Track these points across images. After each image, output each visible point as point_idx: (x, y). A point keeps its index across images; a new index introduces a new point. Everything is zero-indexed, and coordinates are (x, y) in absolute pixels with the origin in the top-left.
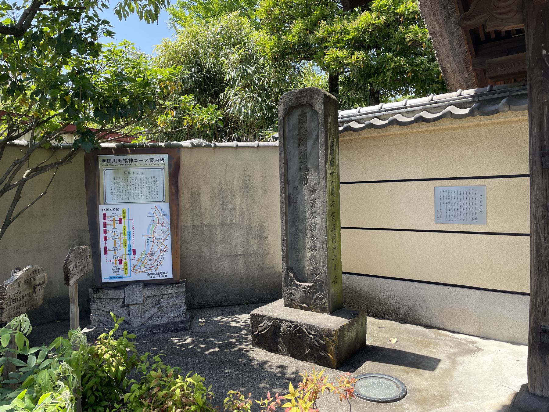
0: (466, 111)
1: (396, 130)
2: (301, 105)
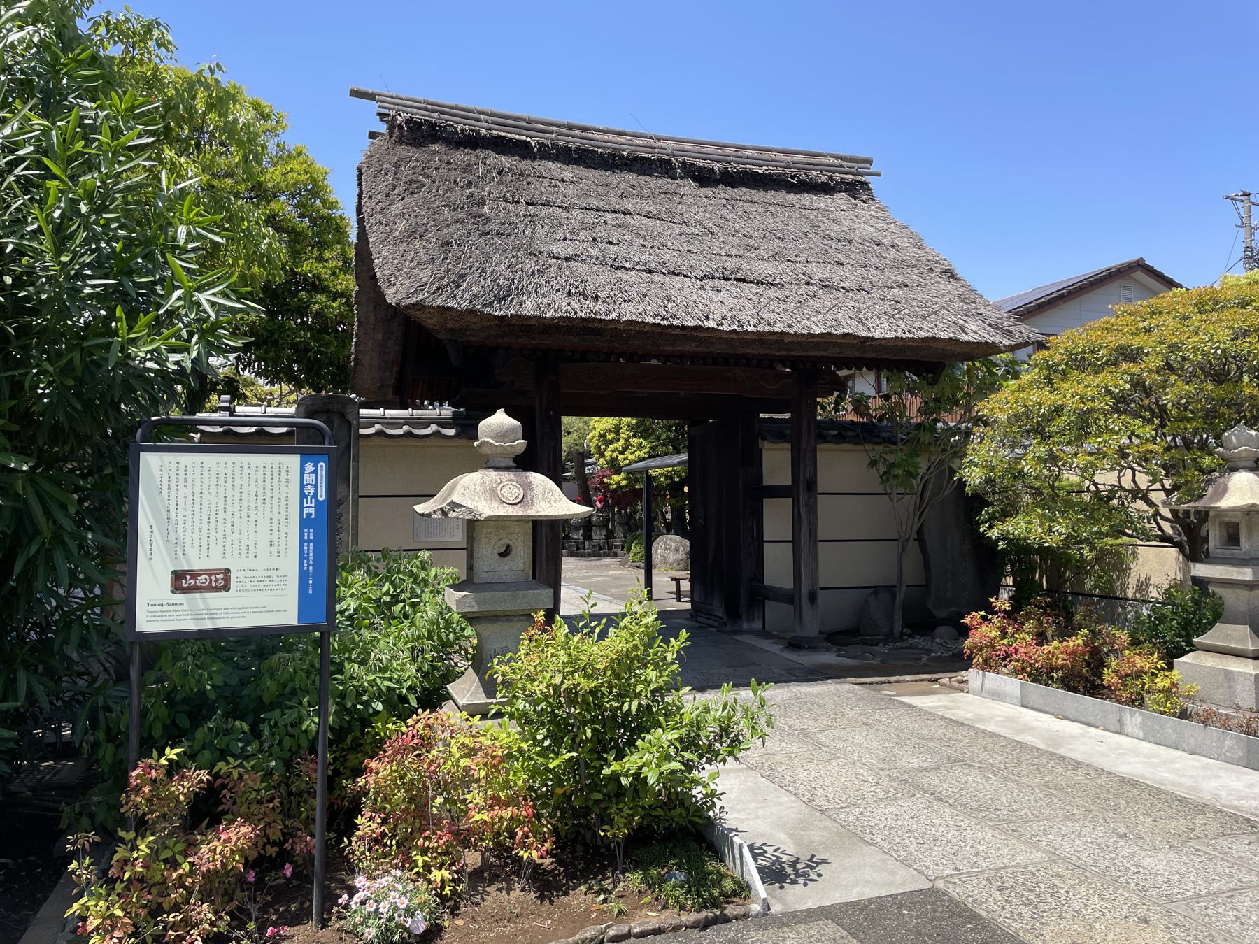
0: (452, 432)
1: (381, 441)
2: (328, 411)
